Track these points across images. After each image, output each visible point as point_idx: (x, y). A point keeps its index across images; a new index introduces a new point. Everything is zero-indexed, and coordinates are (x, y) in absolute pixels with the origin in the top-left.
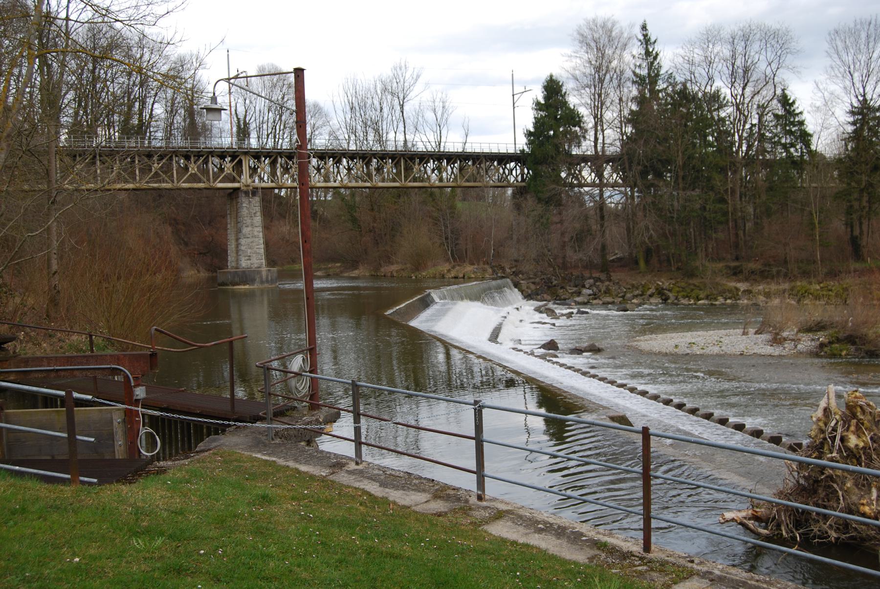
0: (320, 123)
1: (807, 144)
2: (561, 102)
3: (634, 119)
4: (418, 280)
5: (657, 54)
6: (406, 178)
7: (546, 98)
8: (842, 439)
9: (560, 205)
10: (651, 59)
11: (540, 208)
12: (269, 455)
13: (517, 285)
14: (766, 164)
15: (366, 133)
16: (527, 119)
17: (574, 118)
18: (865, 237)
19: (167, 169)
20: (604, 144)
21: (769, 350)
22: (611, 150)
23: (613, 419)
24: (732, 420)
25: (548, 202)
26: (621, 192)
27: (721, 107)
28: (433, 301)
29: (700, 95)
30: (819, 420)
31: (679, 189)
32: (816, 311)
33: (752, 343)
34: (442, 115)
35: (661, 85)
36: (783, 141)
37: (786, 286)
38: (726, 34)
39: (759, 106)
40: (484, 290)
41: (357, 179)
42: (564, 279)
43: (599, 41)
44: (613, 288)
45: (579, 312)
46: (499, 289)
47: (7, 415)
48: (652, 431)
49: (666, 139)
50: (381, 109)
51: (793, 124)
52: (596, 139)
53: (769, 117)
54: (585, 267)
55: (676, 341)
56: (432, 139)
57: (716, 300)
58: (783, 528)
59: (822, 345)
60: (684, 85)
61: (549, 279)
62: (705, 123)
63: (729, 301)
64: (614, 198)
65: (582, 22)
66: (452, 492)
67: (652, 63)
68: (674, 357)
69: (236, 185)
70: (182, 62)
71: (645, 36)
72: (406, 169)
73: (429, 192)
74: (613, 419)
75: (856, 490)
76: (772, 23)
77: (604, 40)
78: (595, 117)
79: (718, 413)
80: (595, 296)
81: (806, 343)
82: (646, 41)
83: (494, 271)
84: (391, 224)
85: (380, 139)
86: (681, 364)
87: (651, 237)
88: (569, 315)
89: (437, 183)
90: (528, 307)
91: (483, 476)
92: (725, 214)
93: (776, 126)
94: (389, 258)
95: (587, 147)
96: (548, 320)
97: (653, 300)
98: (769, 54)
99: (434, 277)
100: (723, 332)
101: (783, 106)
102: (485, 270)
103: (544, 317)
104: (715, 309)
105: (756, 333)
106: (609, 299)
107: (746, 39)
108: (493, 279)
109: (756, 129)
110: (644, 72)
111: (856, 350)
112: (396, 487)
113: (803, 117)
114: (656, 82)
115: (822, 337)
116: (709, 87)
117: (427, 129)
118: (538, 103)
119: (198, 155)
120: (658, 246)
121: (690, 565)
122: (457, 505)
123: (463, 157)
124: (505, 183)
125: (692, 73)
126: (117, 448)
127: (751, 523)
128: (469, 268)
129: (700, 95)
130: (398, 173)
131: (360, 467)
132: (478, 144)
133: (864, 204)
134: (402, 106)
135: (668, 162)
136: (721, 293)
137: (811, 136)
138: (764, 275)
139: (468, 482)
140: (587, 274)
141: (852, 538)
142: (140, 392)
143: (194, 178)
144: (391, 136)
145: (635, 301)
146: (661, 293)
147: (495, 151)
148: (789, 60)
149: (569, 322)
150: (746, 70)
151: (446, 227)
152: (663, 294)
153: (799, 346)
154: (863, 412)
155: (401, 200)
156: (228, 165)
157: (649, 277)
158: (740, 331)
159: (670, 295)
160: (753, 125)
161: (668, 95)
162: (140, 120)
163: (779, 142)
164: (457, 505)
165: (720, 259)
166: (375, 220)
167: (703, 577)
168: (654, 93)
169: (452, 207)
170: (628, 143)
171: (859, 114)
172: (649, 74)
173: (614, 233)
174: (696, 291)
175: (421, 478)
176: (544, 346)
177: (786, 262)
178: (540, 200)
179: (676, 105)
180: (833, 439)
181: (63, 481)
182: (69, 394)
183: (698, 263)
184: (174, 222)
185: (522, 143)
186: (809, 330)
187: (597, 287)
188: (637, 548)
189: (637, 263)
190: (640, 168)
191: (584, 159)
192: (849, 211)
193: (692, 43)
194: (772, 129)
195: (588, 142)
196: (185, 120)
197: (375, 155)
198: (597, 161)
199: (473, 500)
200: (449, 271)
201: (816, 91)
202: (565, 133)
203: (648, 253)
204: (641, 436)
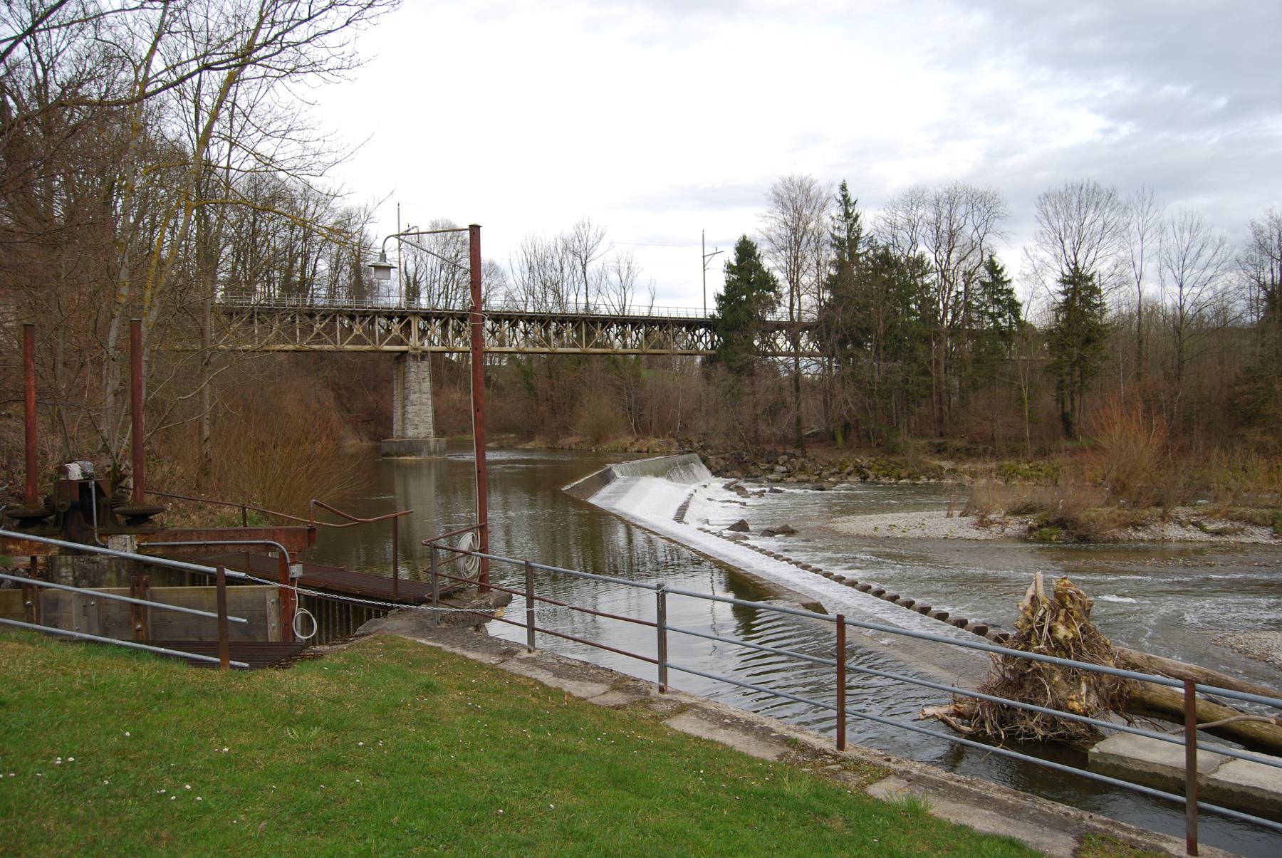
0: (495, 282)
1: (1016, 314)
3: (832, 284)
5: (857, 216)
7: (739, 260)
8: (1050, 630)
9: (752, 375)
10: (850, 221)
11: (731, 378)
12: (434, 640)
14: (973, 334)
16: (718, 283)
17: (767, 282)
18: (1077, 413)
19: (330, 330)
20: (800, 309)
21: (975, 534)
23: (806, 606)
25: (739, 371)
27: (925, 273)
28: (614, 477)
29: (903, 259)
32: (1025, 492)
33: (958, 526)
35: (862, 249)
36: (991, 310)
37: (994, 465)
38: (930, 196)
39: (965, 273)
41: (534, 343)
42: (756, 454)
43: (795, 202)
44: (809, 465)
45: (772, 491)
47: (152, 593)
49: (866, 307)
51: (1001, 292)
53: (976, 285)
54: (779, 442)
55: (876, 523)
56: (616, 303)
57: (918, 479)
59: (1031, 529)
60: (886, 248)
62: (908, 291)
63: (932, 481)
64: (810, 368)
65: (778, 181)
66: (632, 684)
67: (852, 225)
68: (871, 540)
69: (404, 348)
70: (349, 215)
71: (845, 196)
72: (587, 334)
74: (806, 606)
76: (979, 185)
77: (801, 200)
78: (791, 282)
80: (789, 474)
81: (1015, 526)
82: (846, 202)
84: (568, 391)
86: (887, 549)
87: (849, 411)
88: (761, 494)
90: (718, 484)
92: (929, 387)
93: (983, 294)
95: (781, 313)
96: (739, 499)
97: (850, 479)
101: (991, 273)
102: (670, 444)
103: (732, 495)
104: (920, 490)
105: (961, 515)
106: (805, 477)
107: (952, 200)
109: (962, 298)
110: (844, 235)
111: (1068, 534)
112: (571, 678)
115: (1031, 520)
117: (611, 292)
118: (730, 266)
119: (364, 315)
121: (886, 764)
122: (637, 697)
123: (649, 322)
125: (894, 236)
126: (270, 630)
127: (952, 720)
128: (654, 442)
129: (903, 259)
130: (579, 339)
131: (533, 655)
132: (666, 308)
134: (584, 267)
135: (869, 331)
136: (925, 472)
137: (1020, 305)
138: (970, 453)
139: (649, 673)
142: (296, 571)
144: (572, 298)
145: (831, 479)
146: (859, 470)
147: (674, 315)
148: (996, 224)
149: (762, 501)
152: (863, 472)
153: (1007, 530)
155: (582, 367)
161: (868, 259)
163: (986, 312)
164: (637, 697)
165: (923, 436)
166: (553, 388)
167: (900, 777)
168: (854, 257)
169: (637, 376)
170: (826, 309)
171: (1070, 283)
174: (898, 470)
176: (732, 528)
177: (993, 439)
178: (731, 369)
181: (212, 664)
182: (221, 570)
183: (899, 440)
184: (336, 387)
185: (712, 308)
186: (1017, 513)
187: (792, 464)
189: (834, 438)
191: (779, 326)
192: (1060, 387)
193: (895, 206)
194: (980, 297)
196: (350, 278)
197: (554, 318)
198: (793, 328)
199: (655, 692)
200: (632, 444)
201: (1025, 257)
202: (759, 298)
203: (846, 428)
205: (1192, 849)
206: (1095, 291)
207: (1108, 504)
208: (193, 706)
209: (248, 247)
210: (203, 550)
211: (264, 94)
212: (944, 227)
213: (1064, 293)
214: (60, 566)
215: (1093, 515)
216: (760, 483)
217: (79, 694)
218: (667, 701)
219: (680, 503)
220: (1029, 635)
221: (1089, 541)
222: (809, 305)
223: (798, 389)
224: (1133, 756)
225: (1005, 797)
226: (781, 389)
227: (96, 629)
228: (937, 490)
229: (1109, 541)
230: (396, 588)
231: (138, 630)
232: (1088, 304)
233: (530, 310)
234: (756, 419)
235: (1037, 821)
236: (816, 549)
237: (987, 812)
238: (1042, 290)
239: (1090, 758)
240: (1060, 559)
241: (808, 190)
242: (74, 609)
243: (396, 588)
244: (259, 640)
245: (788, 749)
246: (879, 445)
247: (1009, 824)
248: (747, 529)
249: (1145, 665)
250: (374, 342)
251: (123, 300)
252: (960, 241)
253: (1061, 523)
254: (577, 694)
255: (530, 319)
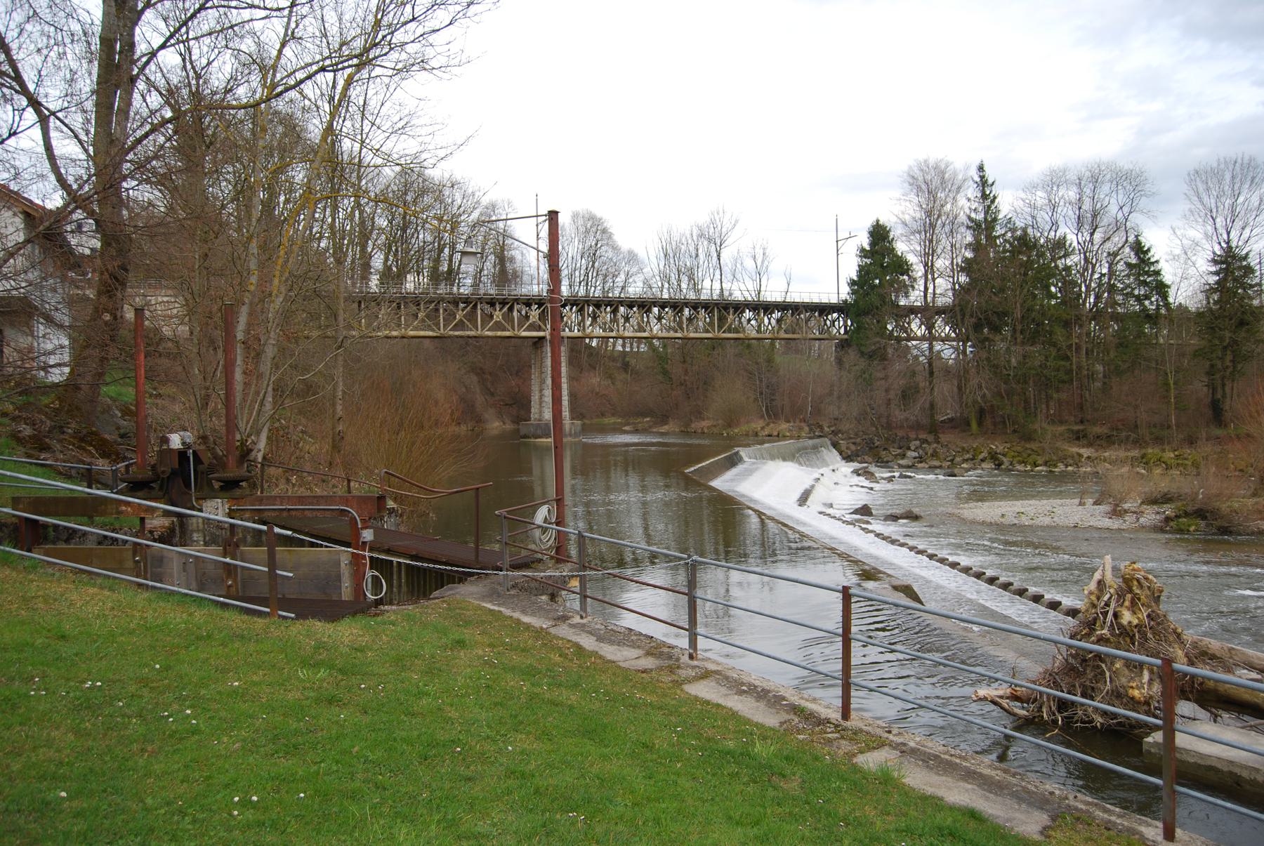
0: (634, 270)
1: (1165, 296)
2: (888, 249)
3: (968, 267)
4: (729, 437)
5: (995, 198)
6: (720, 327)
7: (872, 244)
8: (1116, 615)
9: (885, 359)
10: (988, 202)
11: (863, 363)
12: (499, 605)
13: (835, 445)
14: (1116, 317)
15: (679, 280)
16: (851, 268)
17: (901, 266)
18: (1228, 401)
19: (471, 316)
20: (934, 294)
21: (1107, 523)
22: (940, 301)
23: (896, 588)
24: (1048, 596)
25: (871, 356)
26: (952, 347)
27: (1066, 256)
28: (740, 460)
29: (1042, 241)
30: (1091, 593)
31: (1016, 344)
32: (1161, 482)
33: (1091, 515)
34: (763, 262)
35: (999, 231)
36: (1136, 292)
37: (1135, 453)
38: (1072, 176)
39: (1109, 254)
40: (799, 450)
41: (669, 329)
42: (887, 439)
43: (931, 186)
44: (941, 451)
45: (901, 476)
46: (815, 448)
47: (242, 553)
48: (852, 591)
49: (1002, 290)
50: (697, 255)
51: (1148, 273)
52: (926, 289)
53: (1121, 266)
54: (912, 428)
55: (1003, 511)
56: (751, 288)
57: (1056, 466)
58: (1044, 710)
59: (1168, 519)
60: (1024, 230)
61: (871, 439)
62: (1045, 275)
63: (1070, 468)
64: (947, 352)
65: (912, 163)
66: (666, 650)
67: (989, 207)
68: (999, 527)
69: (541, 334)
70: (493, 206)
71: (982, 177)
72: (720, 319)
73: (745, 342)
74: (896, 588)
75: (1127, 672)
76: (1125, 164)
77: (936, 182)
78: (926, 265)
79: (1033, 590)
80: (921, 459)
81: (1151, 516)
82: (983, 183)
83: (811, 430)
84: (704, 376)
85: (698, 291)
86: (1011, 537)
87: (984, 396)
88: (890, 479)
89: (754, 334)
90: (846, 468)
91: (696, 635)
92: (1069, 372)
93: (1128, 276)
94: (700, 413)
95: (915, 297)
96: (866, 483)
97: (984, 465)
98: (1120, 197)
99: (747, 435)
100: (1059, 501)
101: (1136, 254)
102: (801, 429)
103: (862, 481)
104: (1057, 479)
105: (1095, 503)
106: (936, 463)
107: (1095, 180)
108: (810, 438)
109: (1105, 279)
110: (980, 217)
111: (1207, 525)
112: (611, 642)
113: (1159, 267)
114: (993, 228)
115: (1169, 510)
116: (1052, 233)
117: (746, 278)
118: (863, 250)
119: (503, 303)
120: (992, 406)
121: (887, 735)
122: (667, 663)
123: (783, 307)
124: (826, 336)
125: (1033, 217)
126: (343, 589)
127: (1004, 703)
128: (784, 426)
129: (1042, 241)
130: (711, 324)
131: (584, 621)
132: (799, 294)
133: (1228, 363)
134: (719, 256)
135: (1005, 314)
136: (1062, 459)
137: (1169, 287)
138: (1108, 441)
139: (683, 642)
140: (913, 435)
141: (1119, 724)
142: (368, 535)
143: (498, 326)
144: (707, 284)
145: (964, 465)
146: (993, 457)
147: (816, 300)
148: (1143, 203)
149: (889, 486)
150: (1095, 216)
151: (761, 381)
152: (997, 459)
153: (1142, 520)
154: (1141, 586)
155: (716, 352)
156: (534, 313)
157: (981, 440)
158: (1077, 501)
159: (1005, 459)
160: (1103, 275)
161: (1005, 241)
162: (450, 265)
163: (1131, 294)
164: (667, 663)
165: (1061, 422)
166: (686, 372)
167: (894, 748)
168: (991, 239)
169: (770, 361)
170: (961, 293)
171: (1222, 263)
172: (985, 219)
173: (944, 390)
174: (1034, 457)
175: (641, 634)
176: (856, 512)
177: (1136, 426)
178: (862, 354)
179: (1015, 252)
180: (1105, 614)
181: (260, 614)
182: (271, 529)
183: (1037, 426)
184: (479, 371)
185: (845, 293)
186: (1153, 501)
187: (924, 449)
188: (836, 716)
189: (969, 424)
190: (973, 320)
191: (912, 310)
192: (1211, 372)
193: (1034, 187)
194: (1124, 280)
195: (917, 293)
196: (494, 267)
197: (686, 303)
198: (928, 312)
199: (685, 659)
200: (763, 428)
201: (1173, 237)
202: (891, 283)
203: (981, 414)
204: (840, 595)
205: (1169, 835)
206: (1249, 270)
207: (1254, 495)
208: (226, 646)
209: (399, 239)
210: (285, 514)
211: (373, 90)
212: (1087, 206)
213: (1217, 273)
214: (192, 531)
215: (1236, 505)
216: (891, 469)
217: (132, 632)
218: (694, 667)
219: (807, 486)
220: (1095, 620)
221: (1230, 533)
222: (943, 290)
223: (931, 373)
224: (1188, 747)
225: (993, 773)
226: (914, 374)
227: (194, 585)
228: (1063, 478)
229: (1253, 533)
230: (477, 556)
231: (230, 586)
232: (1245, 287)
233: (666, 296)
234: (889, 402)
235: (1018, 798)
236: (938, 536)
237: (970, 786)
238: (1192, 271)
239: (1145, 747)
240: (1197, 551)
241: (943, 173)
242: (175, 567)
243: (477, 556)
244: (335, 598)
245: (792, 716)
246: (1015, 431)
247: (987, 799)
248: (870, 514)
249: (1226, 656)
250: (438, 325)
251: (252, 288)
252: (1105, 221)
253: (1201, 514)
254: (609, 657)
255: (663, 305)
